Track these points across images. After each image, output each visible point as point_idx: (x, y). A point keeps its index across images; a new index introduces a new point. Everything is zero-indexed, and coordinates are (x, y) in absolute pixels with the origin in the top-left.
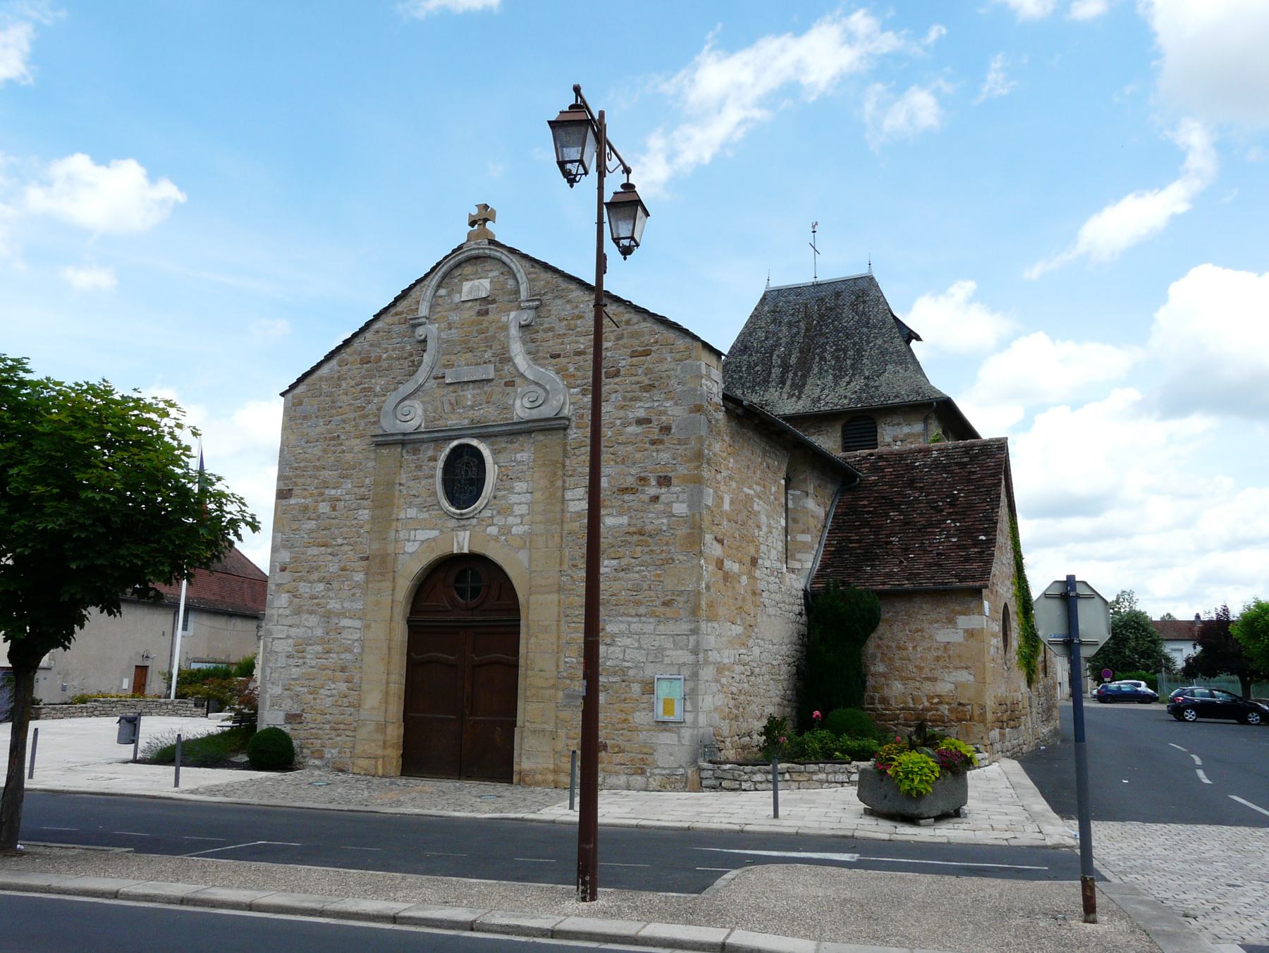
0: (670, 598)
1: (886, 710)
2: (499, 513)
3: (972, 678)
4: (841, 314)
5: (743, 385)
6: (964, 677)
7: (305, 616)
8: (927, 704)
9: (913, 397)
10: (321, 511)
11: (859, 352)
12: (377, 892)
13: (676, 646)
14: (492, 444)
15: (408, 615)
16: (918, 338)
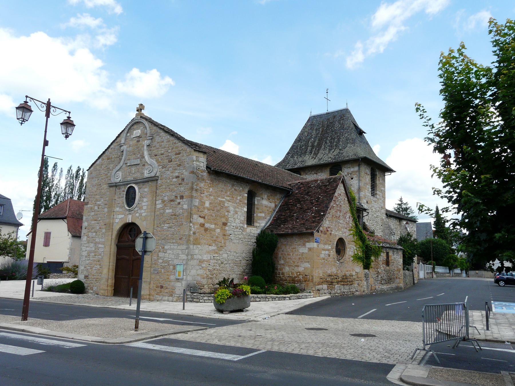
0: (181, 237)
1: (283, 277)
2: (139, 209)
3: (309, 266)
4: (334, 125)
5: (297, 154)
6: (307, 265)
7: (90, 244)
8: (296, 275)
9: (354, 157)
10: (95, 209)
11: (339, 140)
12: (39, 325)
13: (183, 254)
14: (139, 186)
15: (117, 243)
16: (365, 133)
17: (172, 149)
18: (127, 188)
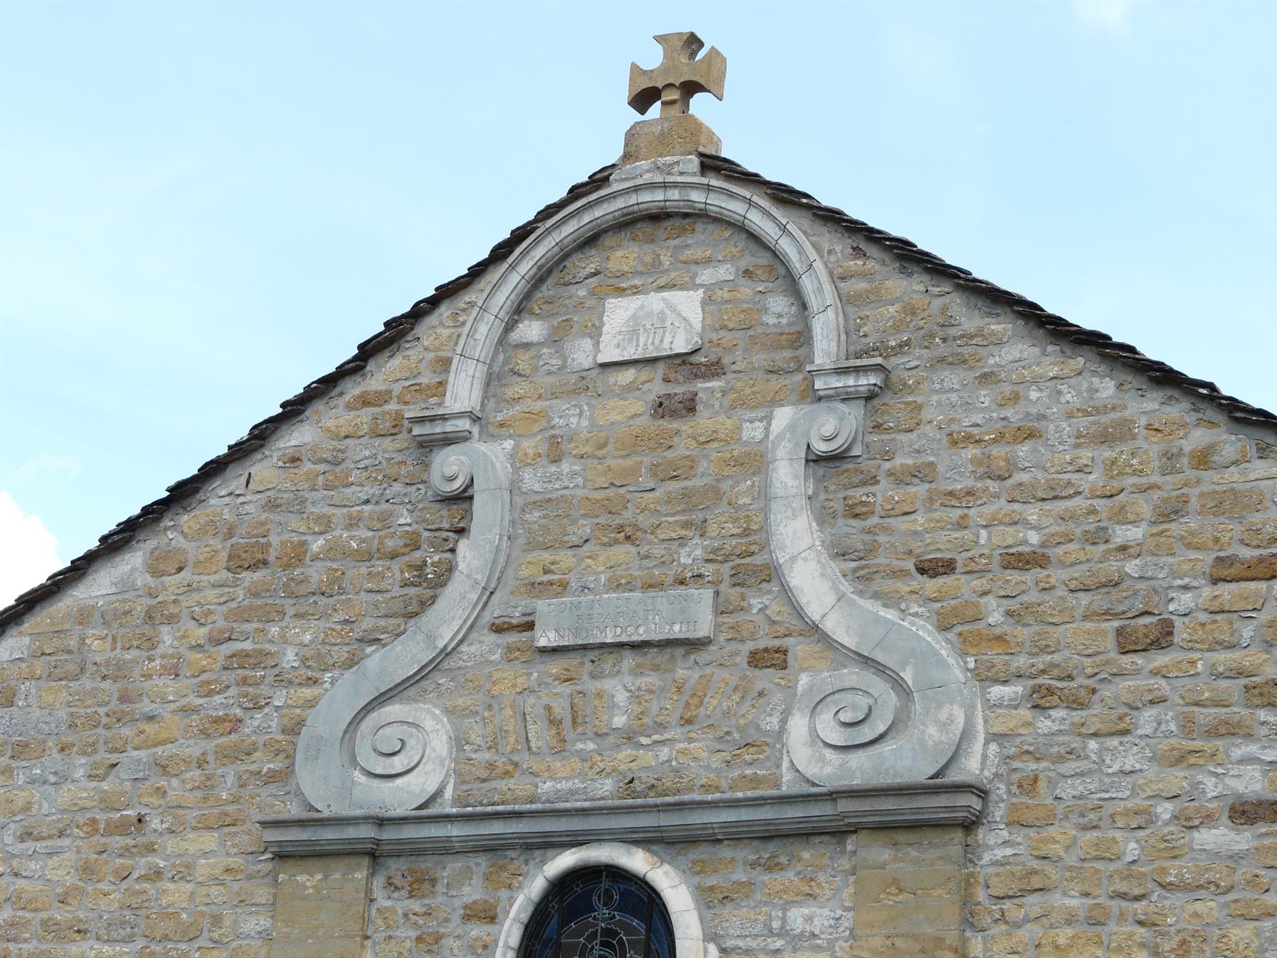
14: (700, 868)
17: (1170, 512)
18: (536, 886)
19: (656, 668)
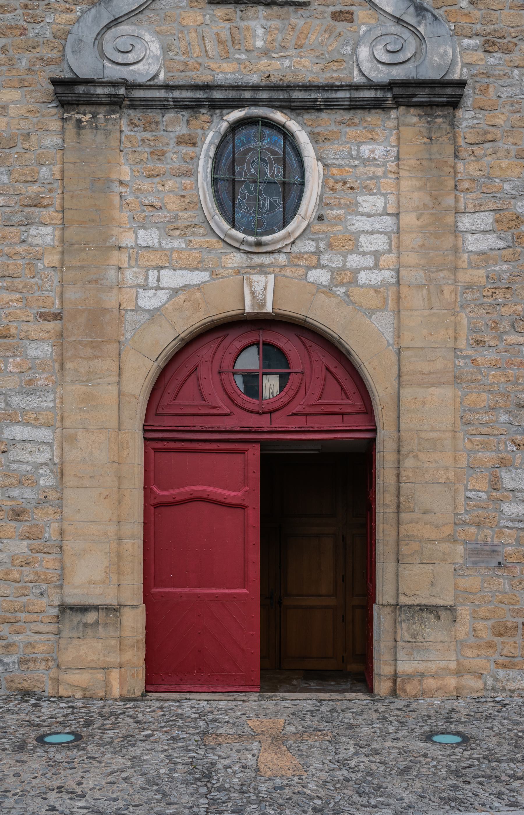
18: (224, 126)
19: (279, 17)
